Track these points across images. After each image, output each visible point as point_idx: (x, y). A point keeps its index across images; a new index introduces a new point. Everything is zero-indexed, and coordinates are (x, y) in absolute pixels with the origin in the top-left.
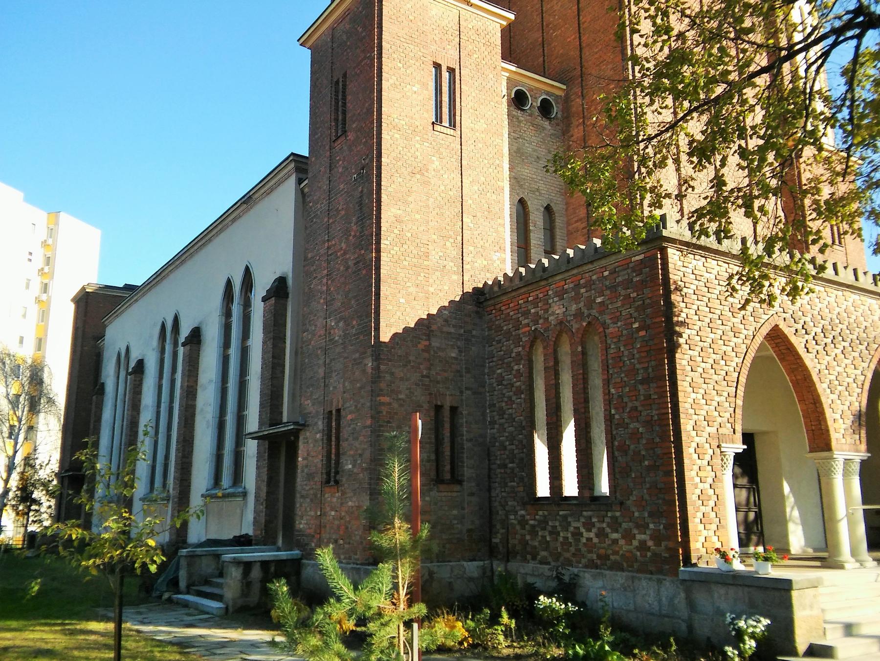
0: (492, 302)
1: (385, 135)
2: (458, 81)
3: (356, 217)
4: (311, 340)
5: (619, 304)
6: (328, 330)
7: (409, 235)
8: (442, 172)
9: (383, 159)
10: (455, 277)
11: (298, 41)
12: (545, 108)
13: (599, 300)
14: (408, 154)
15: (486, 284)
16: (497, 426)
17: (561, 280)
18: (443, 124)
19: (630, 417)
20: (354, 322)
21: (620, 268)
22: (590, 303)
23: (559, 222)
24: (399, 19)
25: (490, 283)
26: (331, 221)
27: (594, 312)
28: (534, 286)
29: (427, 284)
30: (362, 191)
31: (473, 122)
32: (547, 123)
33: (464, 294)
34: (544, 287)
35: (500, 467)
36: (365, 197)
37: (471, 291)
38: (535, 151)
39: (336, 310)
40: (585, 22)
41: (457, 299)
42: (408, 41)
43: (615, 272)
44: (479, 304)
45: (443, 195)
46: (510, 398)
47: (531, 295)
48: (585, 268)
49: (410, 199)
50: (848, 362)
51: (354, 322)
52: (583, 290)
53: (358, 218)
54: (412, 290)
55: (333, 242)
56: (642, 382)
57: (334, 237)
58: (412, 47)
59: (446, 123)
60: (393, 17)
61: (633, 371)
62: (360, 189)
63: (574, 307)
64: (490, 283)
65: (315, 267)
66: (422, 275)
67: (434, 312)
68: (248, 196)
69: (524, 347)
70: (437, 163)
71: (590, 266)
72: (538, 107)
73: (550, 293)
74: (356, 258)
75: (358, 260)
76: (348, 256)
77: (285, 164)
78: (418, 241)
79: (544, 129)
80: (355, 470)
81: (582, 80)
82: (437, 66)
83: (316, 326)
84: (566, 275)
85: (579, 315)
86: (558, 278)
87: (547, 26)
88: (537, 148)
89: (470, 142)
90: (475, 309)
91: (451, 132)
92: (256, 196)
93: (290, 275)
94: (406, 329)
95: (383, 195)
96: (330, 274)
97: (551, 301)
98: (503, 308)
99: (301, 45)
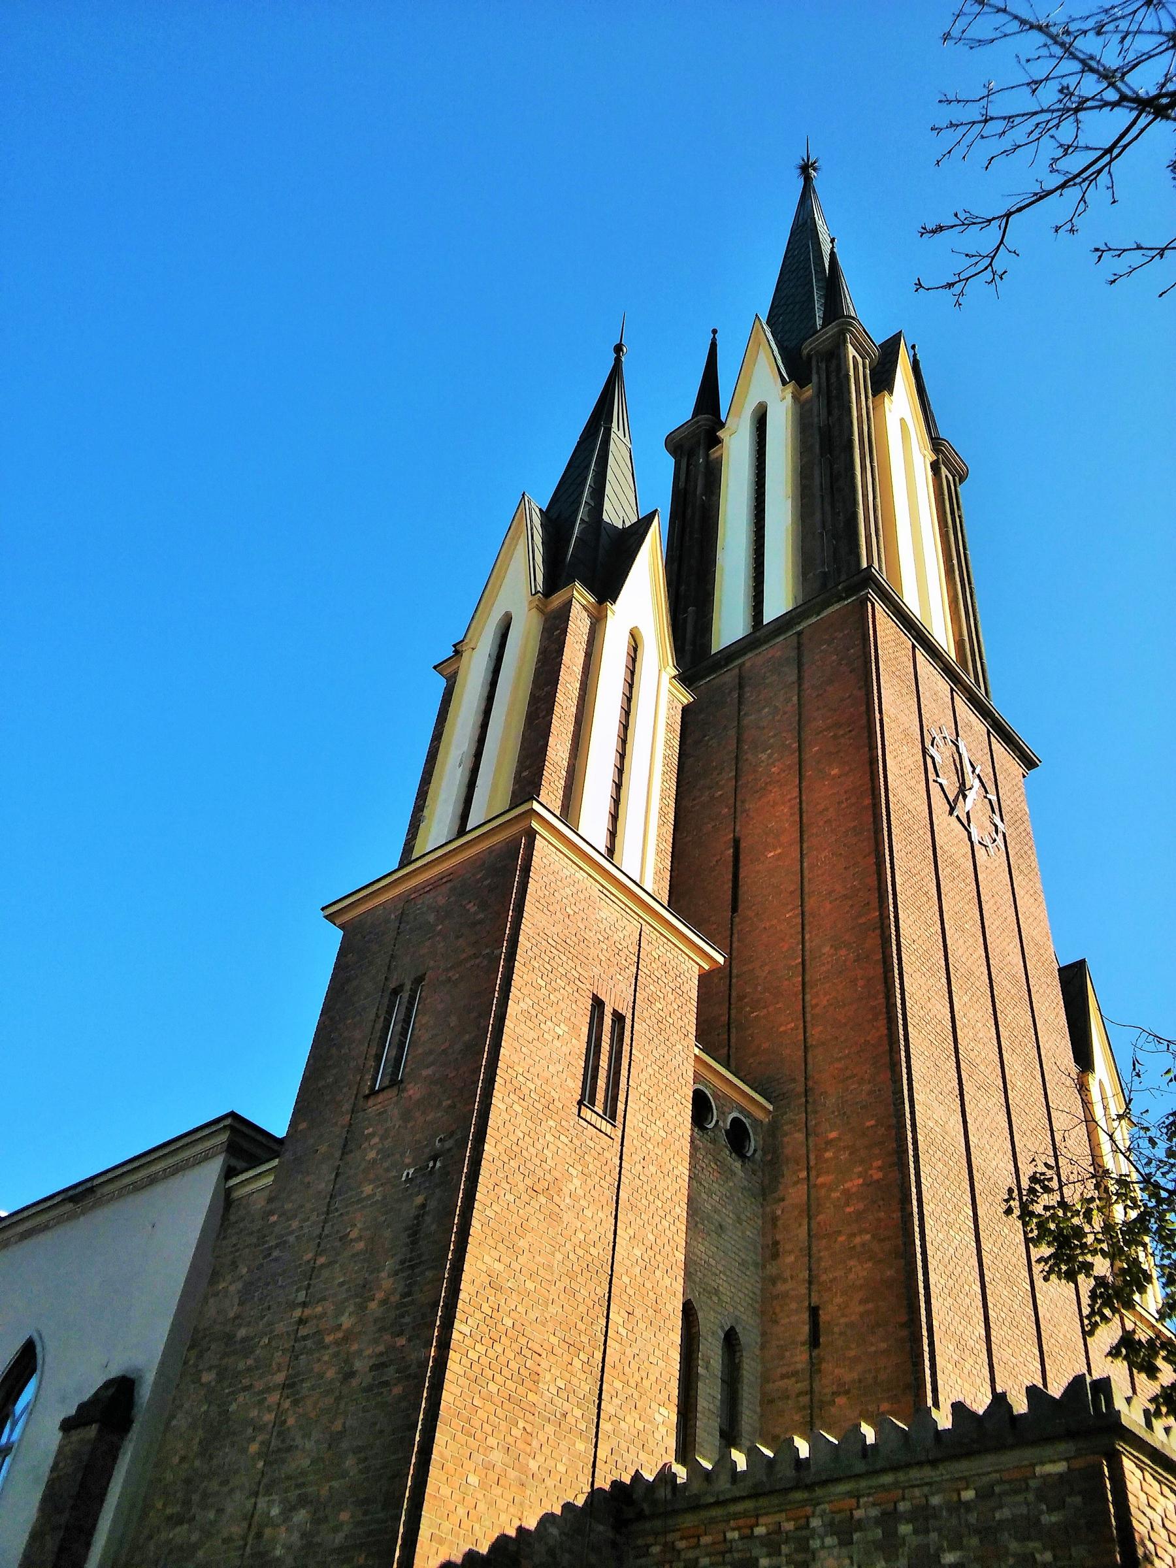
0: (658, 1524)
1: (497, 1101)
2: (627, 1040)
3: (399, 1257)
4: (195, 1547)
6: (255, 1526)
7: (508, 1322)
8: (583, 1203)
9: (486, 1147)
11: (323, 909)
12: (737, 1135)
14: (531, 1149)
15: (637, 1476)
17: (850, 1494)
18: (596, 1109)
20: (344, 1516)
21: (1007, 1487)
23: (750, 1368)
24: (550, 908)
25: (649, 1477)
26: (322, 1260)
28: (775, 1500)
29: (528, 1449)
30: (423, 1206)
31: (645, 1120)
32: (738, 1164)
33: (595, 1494)
34: (804, 1503)
36: (428, 1219)
37: (607, 1487)
38: (716, 1211)
39: (289, 1478)
40: (817, 1005)
41: (580, 1502)
42: (559, 947)
43: (992, 1493)
44: (620, 1524)
45: (580, 1252)
47: (762, 1520)
48: (915, 1474)
49: (522, 1243)
51: (344, 1516)
53: (402, 1262)
54: (497, 1456)
55: (319, 1309)
57: (324, 1299)
58: (565, 959)
60: (542, 901)
62: (419, 1200)
64: (649, 1477)
65: (250, 1362)
66: (521, 1424)
67: (531, 1524)
68: (89, 1185)
70: (577, 1182)
71: (927, 1473)
72: (726, 1131)
73: (815, 1523)
74: (381, 1354)
75: (384, 1359)
76: (355, 1347)
77: (207, 1131)
78: (523, 1341)
79: (733, 1174)
81: (807, 1101)
82: (598, 1004)
84: (863, 1484)
86: (842, 1488)
87: (741, 998)
88: (719, 1207)
89: (636, 1158)
90: (610, 1534)
91: (605, 1126)
92: (107, 1189)
93: (150, 1377)
94: (471, 1556)
95: (474, 1222)
96: (292, 1385)
97: (815, 1544)
98: (681, 1545)
99: (326, 917)
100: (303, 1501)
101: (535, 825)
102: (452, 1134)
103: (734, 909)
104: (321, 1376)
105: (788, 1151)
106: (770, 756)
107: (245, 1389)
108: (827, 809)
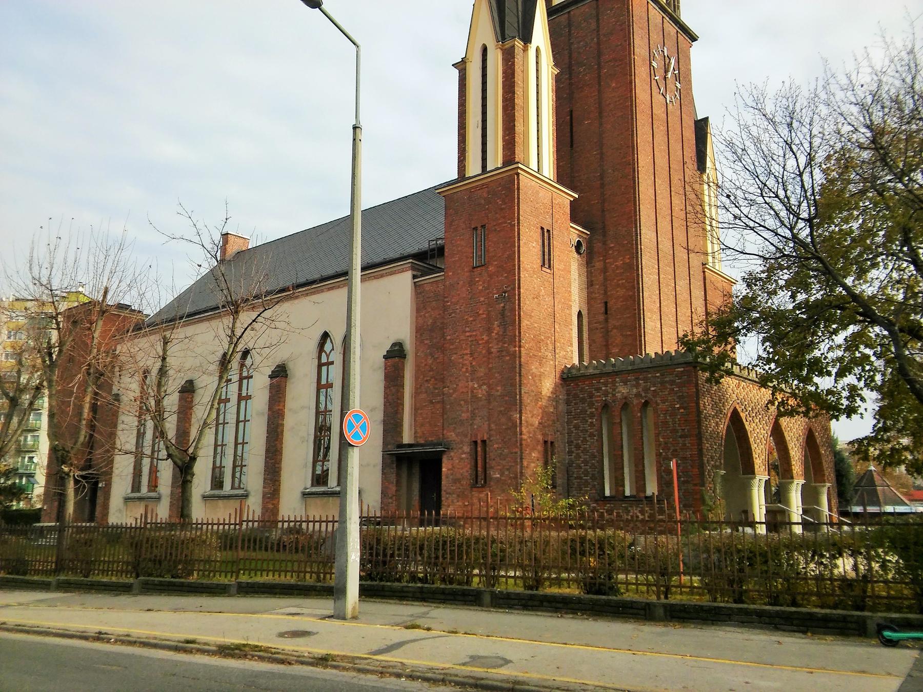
5: (667, 393)
10: (552, 363)
13: (653, 389)
16: (574, 454)
19: (672, 455)
22: (646, 390)
27: (650, 395)
30: (504, 307)
35: (576, 478)
46: (585, 438)
50: (761, 426)
52: (641, 382)
56: (681, 437)
59: (547, 266)
61: (674, 431)
63: (635, 390)
69: (597, 409)
80: (503, 478)
82: (542, 228)
83: (457, 385)
85: (638, 395)
91: (548, 271)
100: (484, 384)
101: (519, 171)
102: (509, 286)
103: (572, 146)
104: (481, 352)
105: (596, 250)
106: (584, 70)
107: (456, 354)
108: (610, 104)
